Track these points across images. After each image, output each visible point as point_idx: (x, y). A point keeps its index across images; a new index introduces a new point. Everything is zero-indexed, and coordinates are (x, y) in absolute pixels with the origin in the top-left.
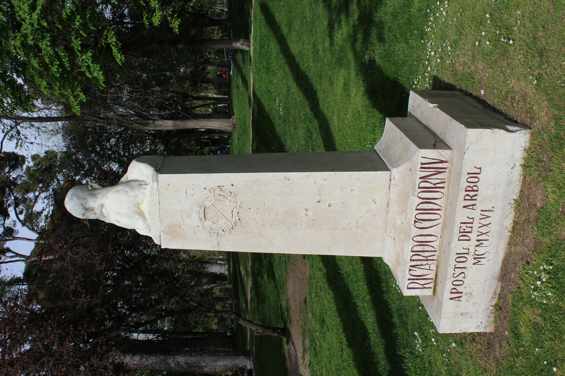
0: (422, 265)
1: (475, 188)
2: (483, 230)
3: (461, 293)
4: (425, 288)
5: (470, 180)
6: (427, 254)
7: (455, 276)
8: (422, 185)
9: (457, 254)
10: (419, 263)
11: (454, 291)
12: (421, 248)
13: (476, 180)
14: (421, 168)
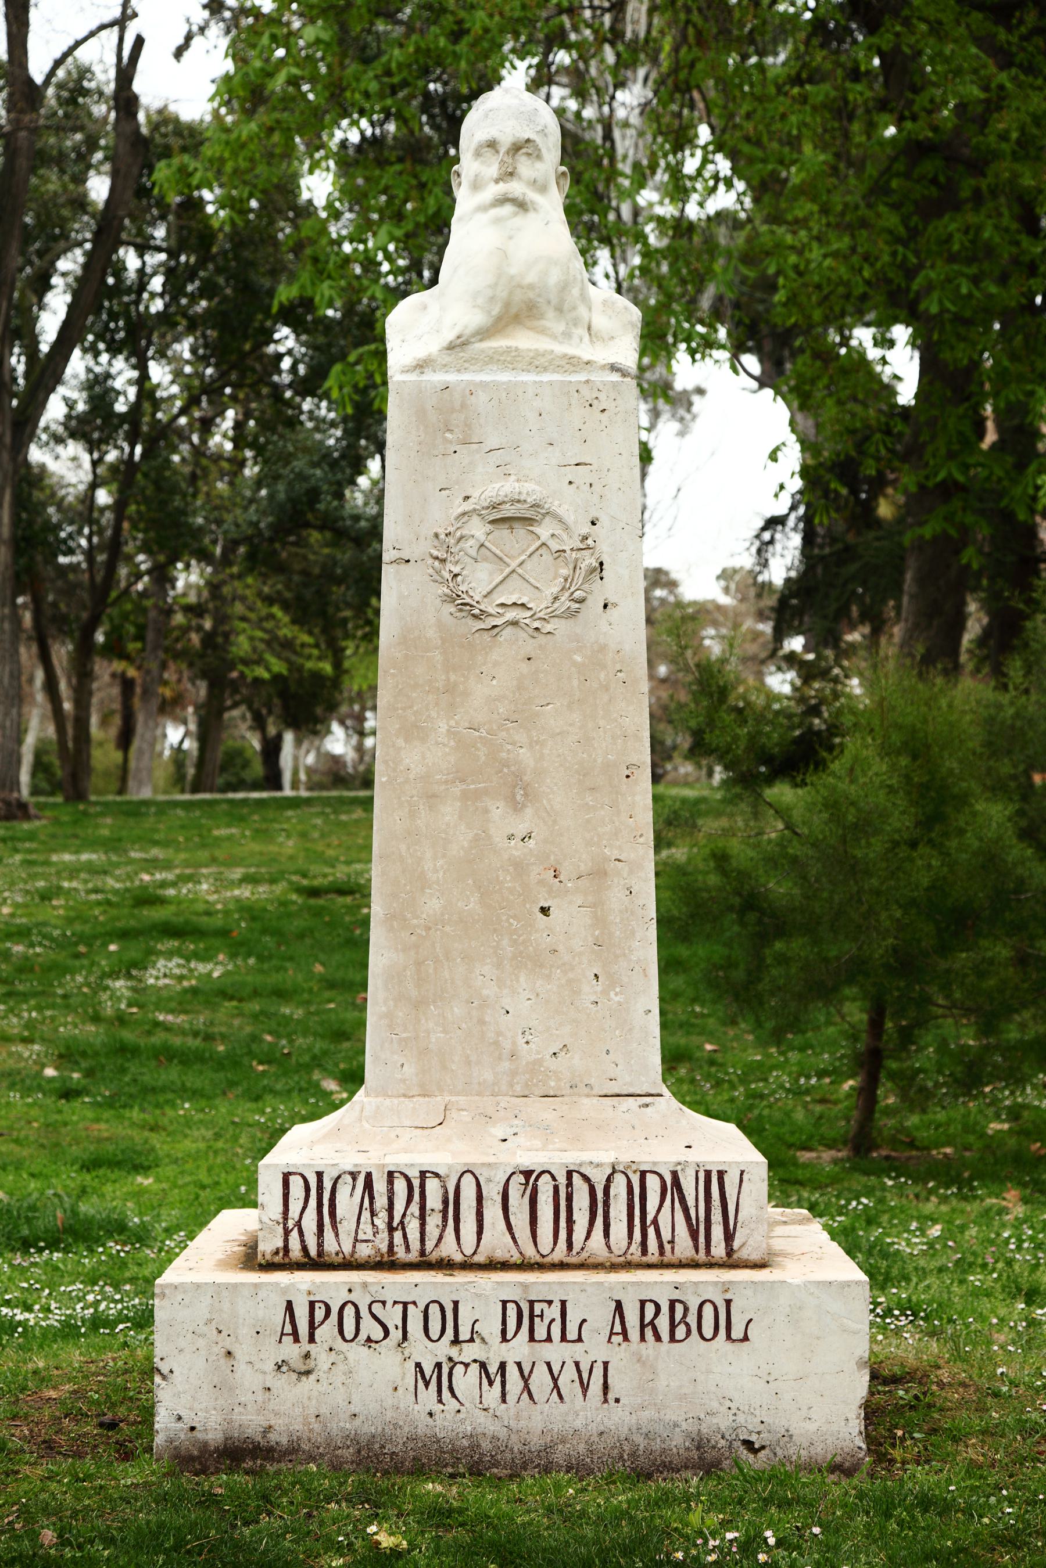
0: (373, 1214)
1: (680, 1332)
2: (540, 1380)
3: (312, 1339)
4: (287, 1233)
6: (413, 1227)
7: (377, 1308)
8: (653, 1184)
9: (456, 1304)
10: (381, 1202)
11: (319, 1314)
12: (434, 1201)
13: (708, 1332)
14: (708, 1174)
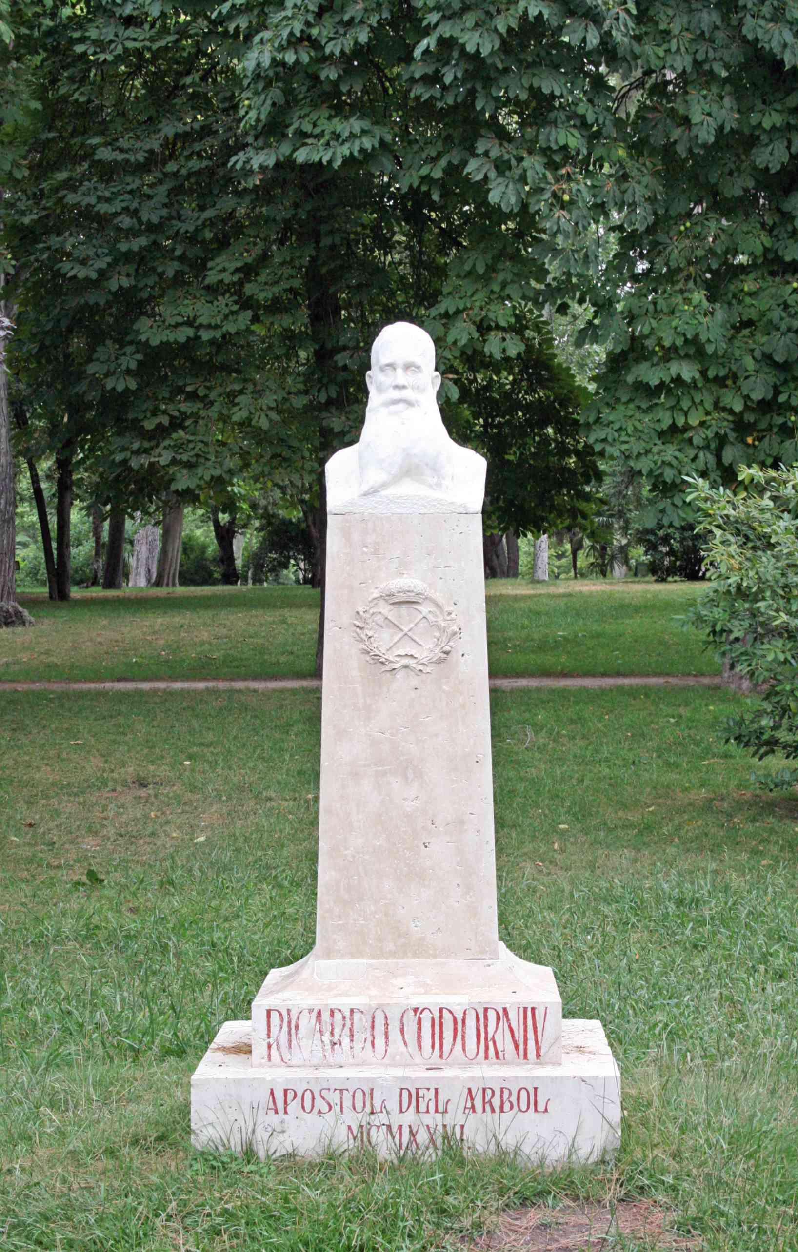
3: (286, 1112)
5: (524, 1094)
14: (525, 1009)
